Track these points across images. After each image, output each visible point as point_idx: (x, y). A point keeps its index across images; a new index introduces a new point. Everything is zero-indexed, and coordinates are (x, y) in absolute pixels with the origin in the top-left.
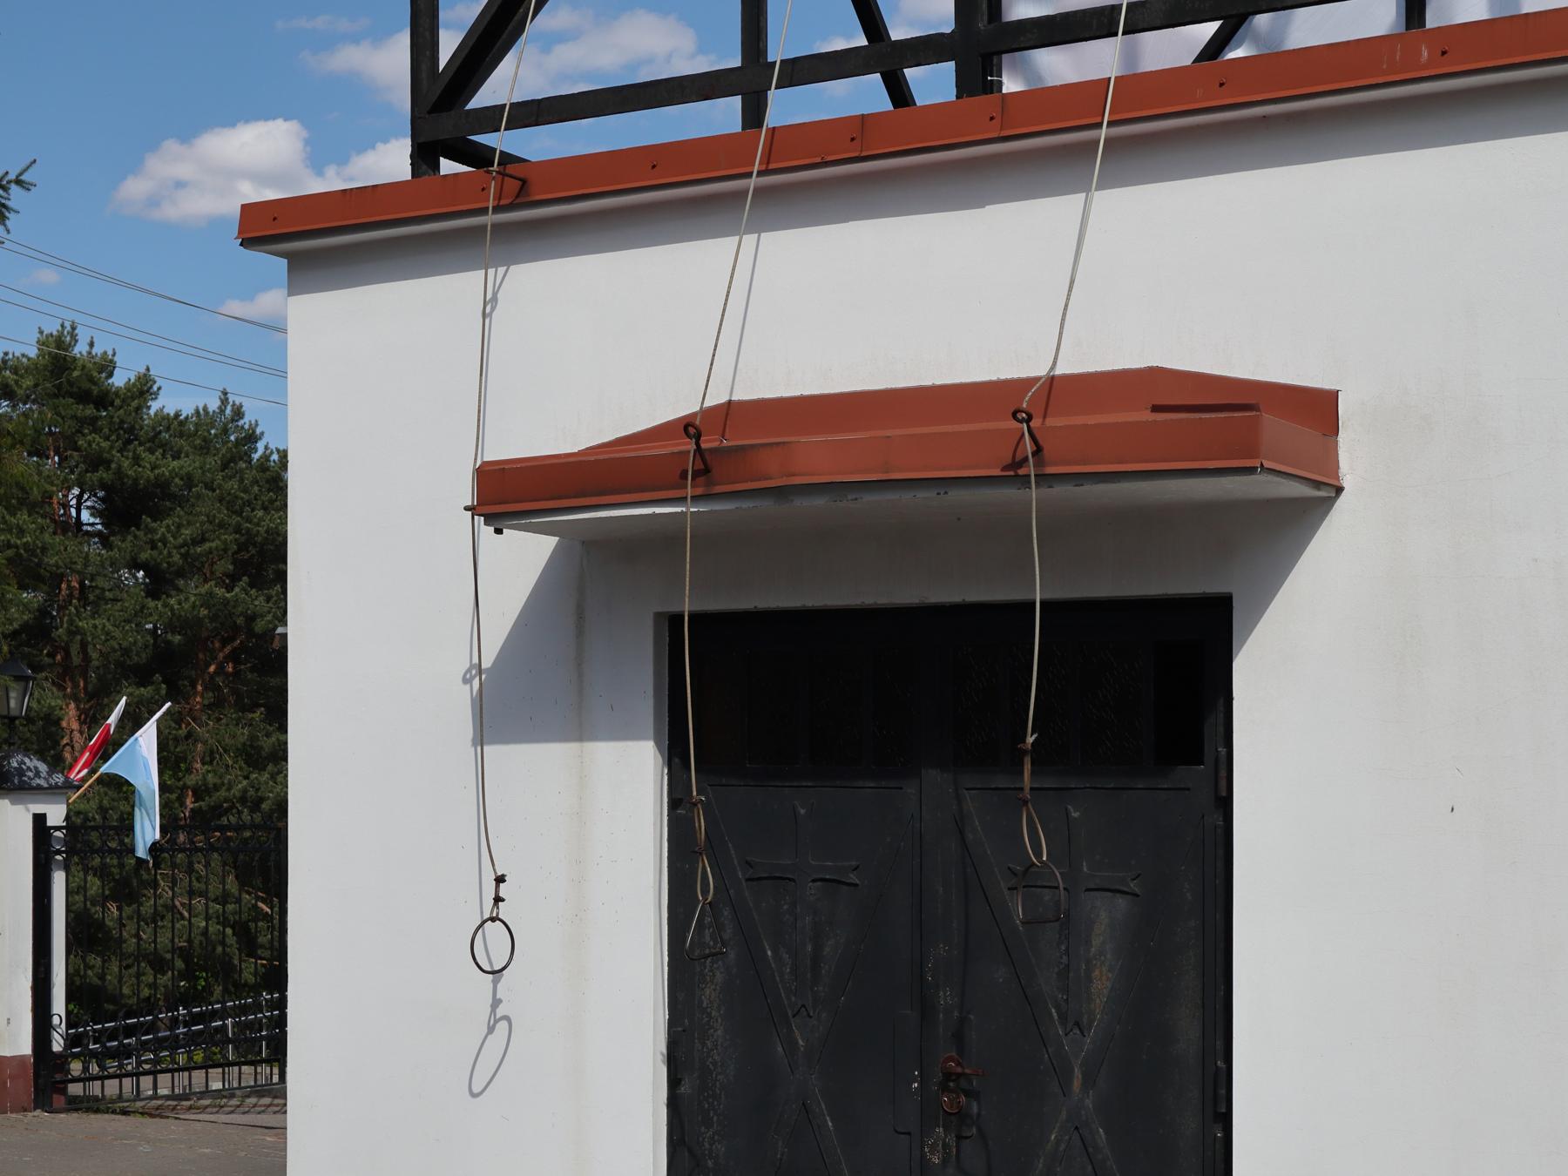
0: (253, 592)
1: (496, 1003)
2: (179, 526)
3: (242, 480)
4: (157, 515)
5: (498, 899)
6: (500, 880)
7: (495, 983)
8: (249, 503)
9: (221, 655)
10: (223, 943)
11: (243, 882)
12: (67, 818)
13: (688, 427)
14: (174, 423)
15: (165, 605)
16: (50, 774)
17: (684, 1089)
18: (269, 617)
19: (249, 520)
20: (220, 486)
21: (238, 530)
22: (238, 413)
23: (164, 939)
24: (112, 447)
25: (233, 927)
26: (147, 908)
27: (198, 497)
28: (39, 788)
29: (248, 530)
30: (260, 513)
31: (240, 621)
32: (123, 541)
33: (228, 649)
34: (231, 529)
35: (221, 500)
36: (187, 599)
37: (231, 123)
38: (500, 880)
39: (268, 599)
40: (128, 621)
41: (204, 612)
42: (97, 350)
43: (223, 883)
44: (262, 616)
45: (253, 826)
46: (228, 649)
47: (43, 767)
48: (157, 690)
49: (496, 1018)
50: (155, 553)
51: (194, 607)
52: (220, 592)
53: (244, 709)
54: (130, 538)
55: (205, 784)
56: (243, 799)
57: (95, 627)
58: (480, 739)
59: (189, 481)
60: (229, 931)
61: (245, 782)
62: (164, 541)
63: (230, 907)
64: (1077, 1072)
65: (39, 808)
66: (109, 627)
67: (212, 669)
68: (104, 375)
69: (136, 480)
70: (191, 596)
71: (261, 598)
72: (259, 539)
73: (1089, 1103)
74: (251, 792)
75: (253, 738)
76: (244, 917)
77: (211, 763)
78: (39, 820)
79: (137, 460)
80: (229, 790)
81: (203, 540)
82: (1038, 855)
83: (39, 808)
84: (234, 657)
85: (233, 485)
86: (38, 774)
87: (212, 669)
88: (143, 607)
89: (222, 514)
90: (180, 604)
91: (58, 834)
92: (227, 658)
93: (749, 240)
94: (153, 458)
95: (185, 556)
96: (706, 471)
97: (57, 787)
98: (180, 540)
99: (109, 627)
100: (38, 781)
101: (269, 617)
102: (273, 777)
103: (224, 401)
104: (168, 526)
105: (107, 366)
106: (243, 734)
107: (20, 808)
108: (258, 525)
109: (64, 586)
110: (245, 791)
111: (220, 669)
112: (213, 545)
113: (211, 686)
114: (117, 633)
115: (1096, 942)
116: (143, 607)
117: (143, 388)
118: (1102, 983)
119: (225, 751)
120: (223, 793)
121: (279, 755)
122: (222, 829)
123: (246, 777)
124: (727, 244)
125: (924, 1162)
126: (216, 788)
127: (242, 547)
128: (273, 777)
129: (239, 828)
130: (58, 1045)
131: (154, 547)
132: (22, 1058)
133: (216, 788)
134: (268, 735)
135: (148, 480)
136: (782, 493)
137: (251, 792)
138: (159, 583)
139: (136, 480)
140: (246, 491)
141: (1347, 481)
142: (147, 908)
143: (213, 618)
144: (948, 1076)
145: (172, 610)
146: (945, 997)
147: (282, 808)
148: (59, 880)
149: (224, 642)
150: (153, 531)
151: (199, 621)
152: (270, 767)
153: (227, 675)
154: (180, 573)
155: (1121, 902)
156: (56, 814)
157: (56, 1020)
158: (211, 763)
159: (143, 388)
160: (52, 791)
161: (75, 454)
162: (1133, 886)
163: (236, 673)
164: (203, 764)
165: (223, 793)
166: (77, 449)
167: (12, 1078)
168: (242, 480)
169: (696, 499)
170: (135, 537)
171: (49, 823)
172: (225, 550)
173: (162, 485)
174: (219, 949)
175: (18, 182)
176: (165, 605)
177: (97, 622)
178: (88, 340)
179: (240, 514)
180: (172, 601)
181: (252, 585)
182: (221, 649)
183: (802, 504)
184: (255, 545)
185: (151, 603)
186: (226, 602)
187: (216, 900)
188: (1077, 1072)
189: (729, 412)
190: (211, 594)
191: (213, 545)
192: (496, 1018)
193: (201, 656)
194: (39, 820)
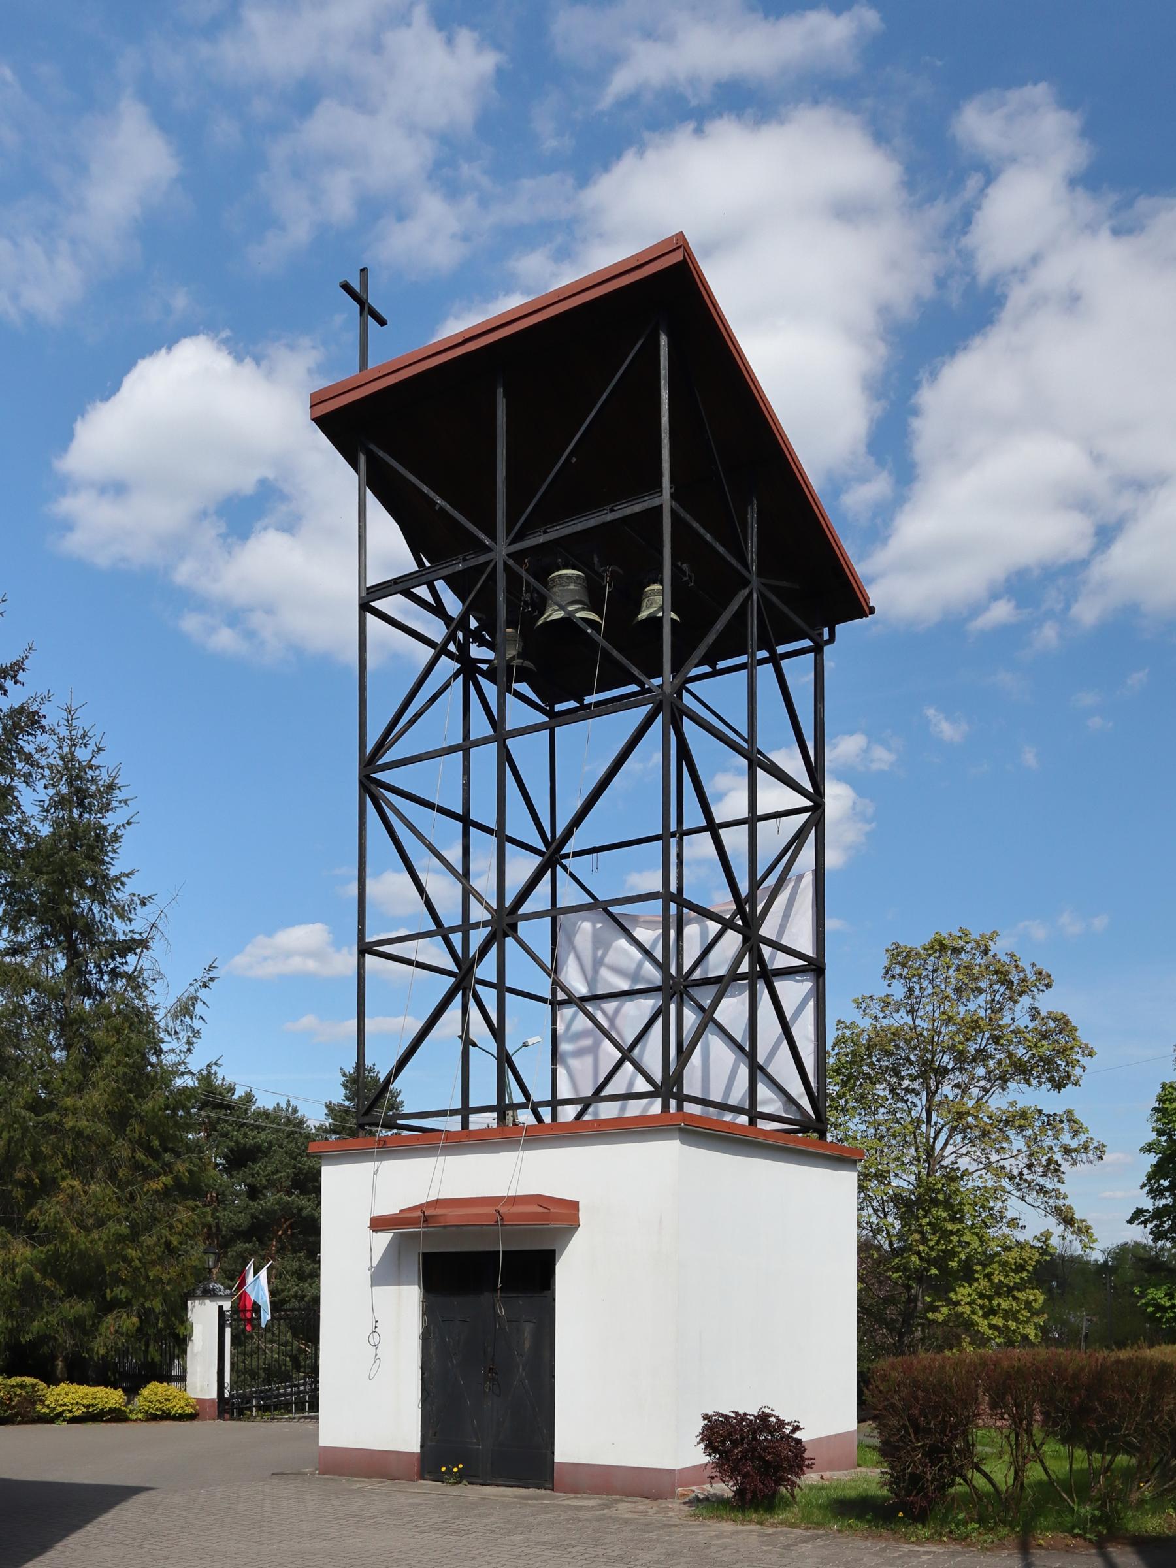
0: (302, 1197)
1: (376, 1355)
2: (265, 1167)
3: (296, 1143)
4: (254, 1161)
5: (376, 1327)
6: (376, 1322)
7: (376, 1349)
8: (300, 1154)
9: (285, 1226)
10: (285, 1365)
11: (295, 1335)
12: (231, 1307)
13: (420, 1207)
14: (265, 1114)
15: (259, 1204)
16: (225, 1290)
17: (425, 1375)
18: (309, 1209)
19: (300, 1162)
20: (285, 1146)
21: (294, 1167)
22: (295, 1110)
23: (255, 1363)
24: (233, 1130)
25: (290, 1357)
26: (248, 1349)
27: (275, 1151)
28: (221, 1295)
29: (299, 1167)
30: (305, 1159)
31: (295, 1211)
32: (238, 1174)
33: (288, 1223)
34: (290, 1167)
35: (286, 1153)
36: (269, 1201)
37: (292, 925)
38: (376, 1322)
39: (309, 1201)
40: (241, 1212)
41: (277, 1207)
42: (226, 1083)
43: (286, 1336)
44: (306, 1209)
45: (299, 1309)
46: (288, 1223)
47: (222, 1288)
48: (254, 1245)
49: (376, 1358)
50: (254, 1179)
51: (272, 1204)
52: (286, 1198)
53: (295, 1251)
54: (241, 1172)
55: (277, 1289)
56: (295, 1296)
57: (224, 1215)
58: (372, 1286)
59: (271, 1143)
60: (288, 1359)
61: (296, 1288)
62: (258, 1174)
63: (289, 1348)
64: (521, 1367)
65: (220, 1303)
66: (231, 1215)
67: (280, 1233)
68: (230, 1094)
69: (245, 1145)
70: (271, 1198)
71: (306, 1200)
72: (305, 1171)
73: (524, 1374)
74: (300, 1292)
75: (301, 1267)
76: (294, 1352)
77: (280, 1279)
78: (221, 1308)
79: (245, 1135)
80: (289, 1291)
81: (277, 1171)
82: (502, 1313)
83: (220, 1303)
84: (291, 1226)
85: (292, 1145)
86: (220, 1290)
87: (280, 1233)
88: (248, 1205)
89: (287, 1159)
90: (265, 1203)
91: (228, 1313)
92: (288, 1227)
93: (441, 1159)
94: (253, 1134)
95: (268, 1180)
96: (427, 1220)
97: (227, 1295)
98: (266, 1173)
99: (231, 1215)
100: (220, 1293)
101: (309, 1209)
102: (310, 1285)
103: (288, 1105)
104: (260, 1167)
105: (232, 1090)
106: (296, 1265)
107: (214, 1303)
108: (304, 1164)
109: (209, 1196)
110: (296, 1292)
111: (285, 1232)
112: (282, 1175)
113: (280, 1239)
114: (235, 1218)
115: (526, 1335)
116: (248, 1205)
117: (249, 1098)
118: (527, 1345)
119: (287, 1273)
120: (286, 1293)
121: (315, 1275)
122: (285, 1310)
123: (297, 1286)
124: (435, 1159)
125: (485, 1391)
126: (283, 1291)
127: (296, 1175)
128: (310, 1285)
129: (292, 1310)
130: (227, 1395)
131: (253, 1177)
132: (213, 1400)
133: (283, 1291)
134: (308, 1265)
135: (251, 1145)
136: (444, 1227)
137: (300, 1292)
138: (254, 1193)
139: (245, 1145)
140: (298, 1148)
141: (581, 1223)
142: (248, 1349)
143: (282, 1210)
144: (490, 1369)
145: (262, 1206)
146: (489, 1349)
147: (316, 1300)
148: (228, 1331)
149: (286, 1220)
150: (254, 1169)
151: (274, 1211)
152: (309, 1280)
153: (288, 1235)
154: (265, 1188)
155: (532, 1324)
156: (227, 1305)
157: (226, 1385)
158: (280, 1279)
159: (249, 1098)
160: (226, 1297)
161: (216, 1133)
162: (534, 1321)
163: (292, 1234)
164: (276, 1278)
165: (286, 1293)
166: (216, 1131)
167: (210, 1407)
168: (296, 1143)
169: (423, 1227)
170: (244, 1172)
171: (224, 1309)
172: (288, 1177)
173: (258, 1148)
174: (283, 1368)
175: (216, 1064)
176: (259, 1204)
177: (225, 1213)
178: (111, 823)
179: (295, 1159)
180: (262, 1202)
181: (301, 1193)
182: (285, 1223)
183: (449, 1229)
184: (303, 1174)
185: (252, 1204)
186: (288, 1202)
187: (282, 1345)
188: (521, 1367)
189: (437, 1203)
190: (281, 1198)
191: (282, 1175)
192: (376, 1358)
193: (275, 1228)
194: (221, 1308)
